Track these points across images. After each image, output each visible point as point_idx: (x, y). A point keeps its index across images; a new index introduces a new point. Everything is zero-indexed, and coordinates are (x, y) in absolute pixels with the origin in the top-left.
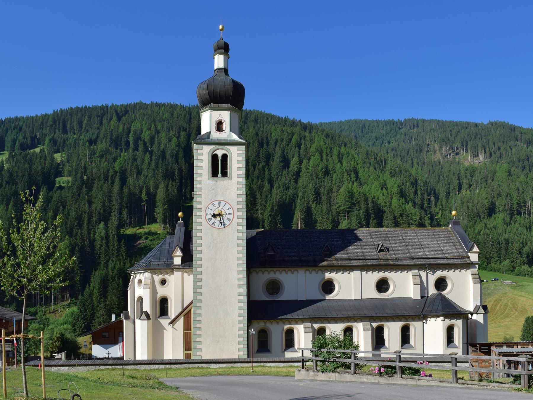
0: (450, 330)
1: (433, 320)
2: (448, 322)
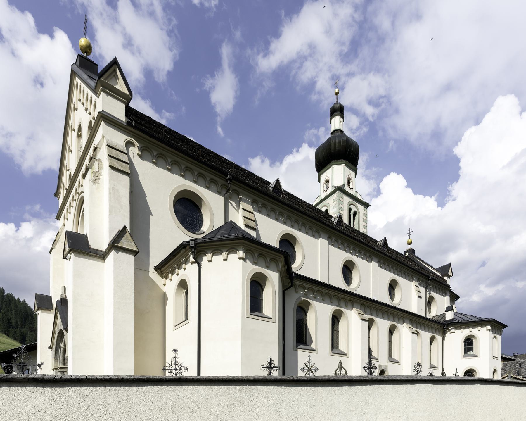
0: (257, 286)
1: (218, 259)
2: (252, 268)
